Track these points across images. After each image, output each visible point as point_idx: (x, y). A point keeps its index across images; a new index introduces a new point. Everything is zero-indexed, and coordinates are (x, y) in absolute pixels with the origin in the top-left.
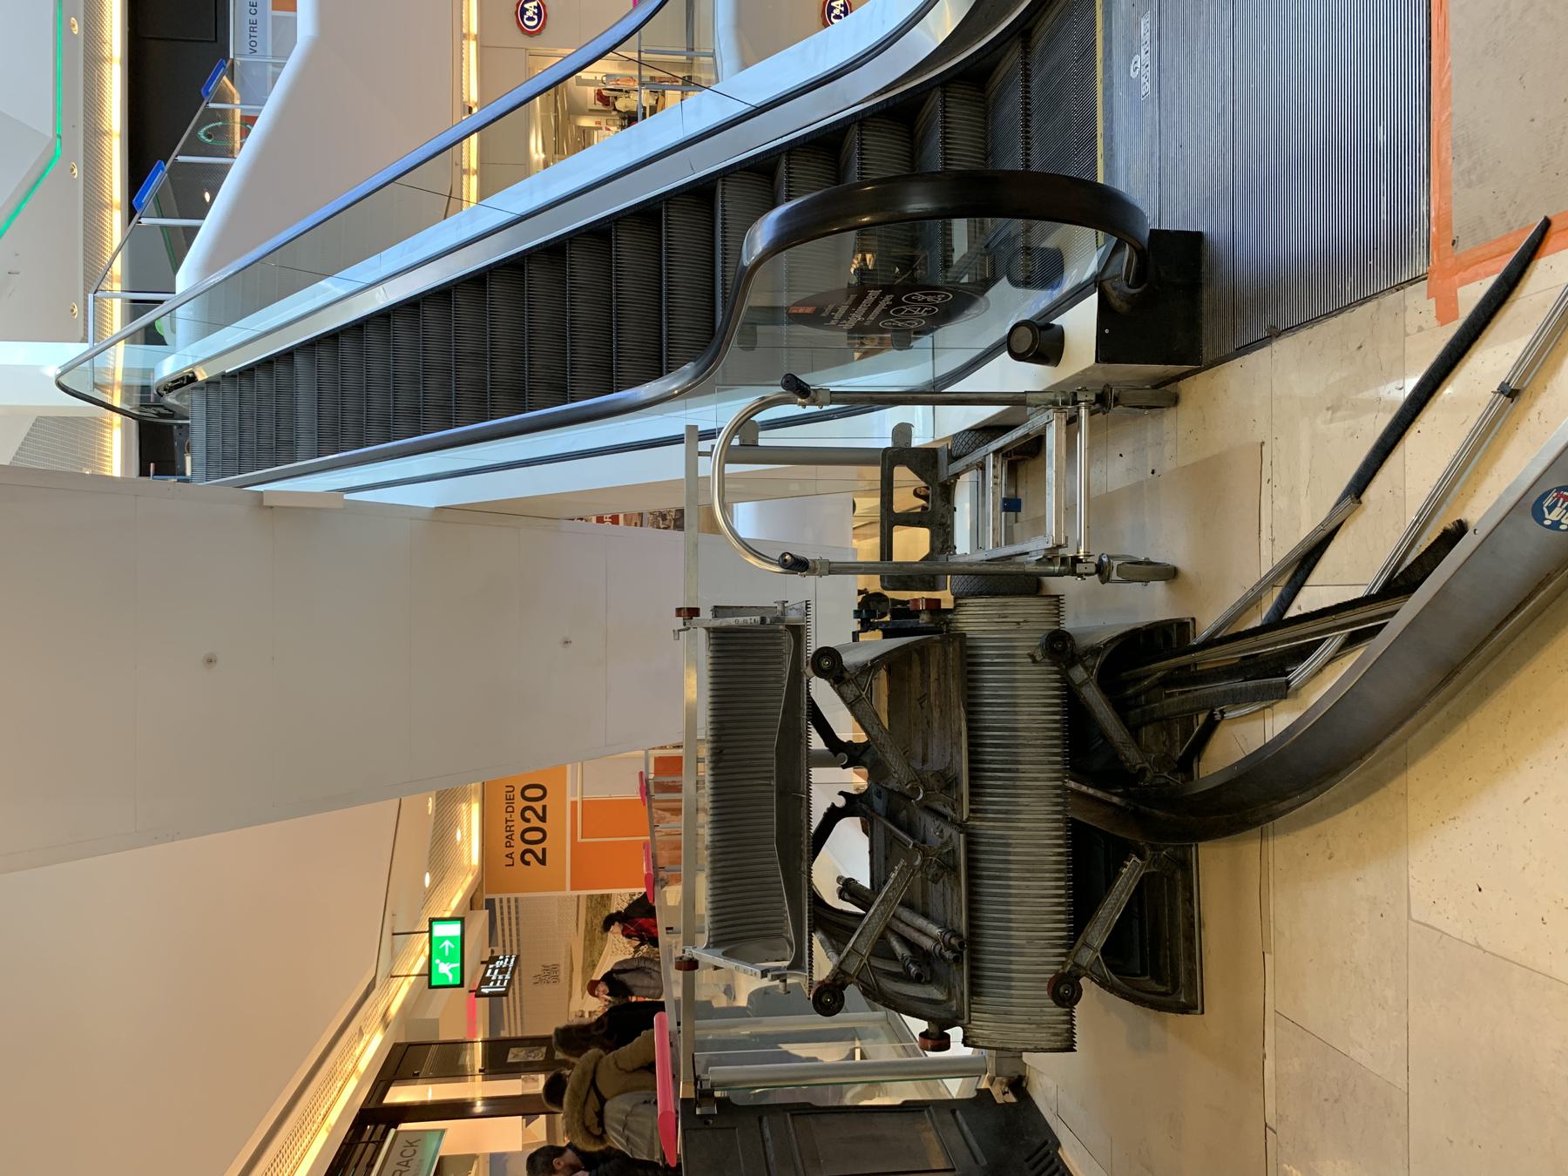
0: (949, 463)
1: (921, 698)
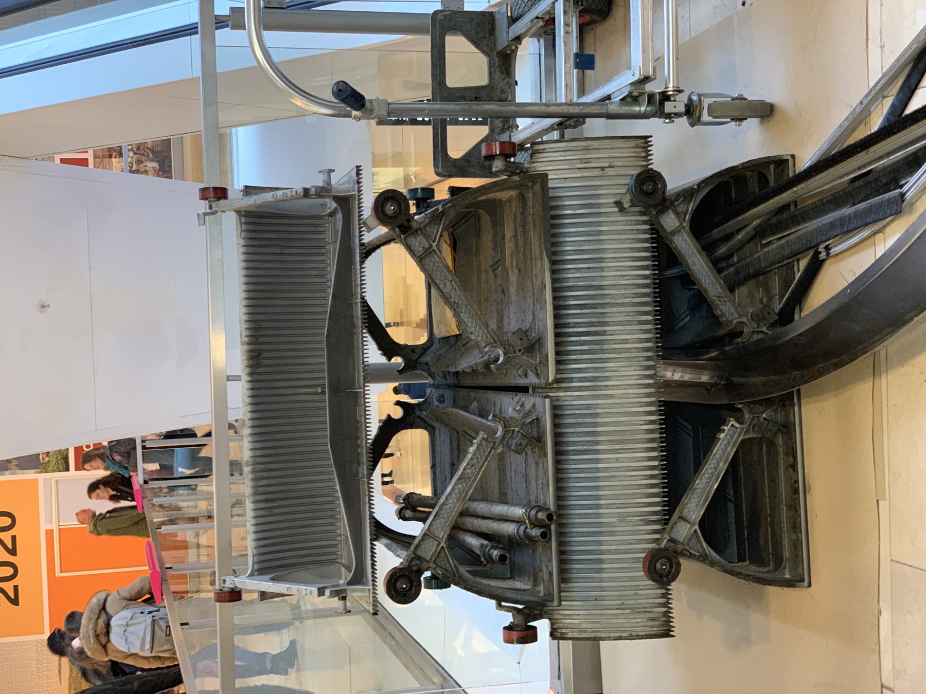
0: (509, 25)
1: (494, 265)
